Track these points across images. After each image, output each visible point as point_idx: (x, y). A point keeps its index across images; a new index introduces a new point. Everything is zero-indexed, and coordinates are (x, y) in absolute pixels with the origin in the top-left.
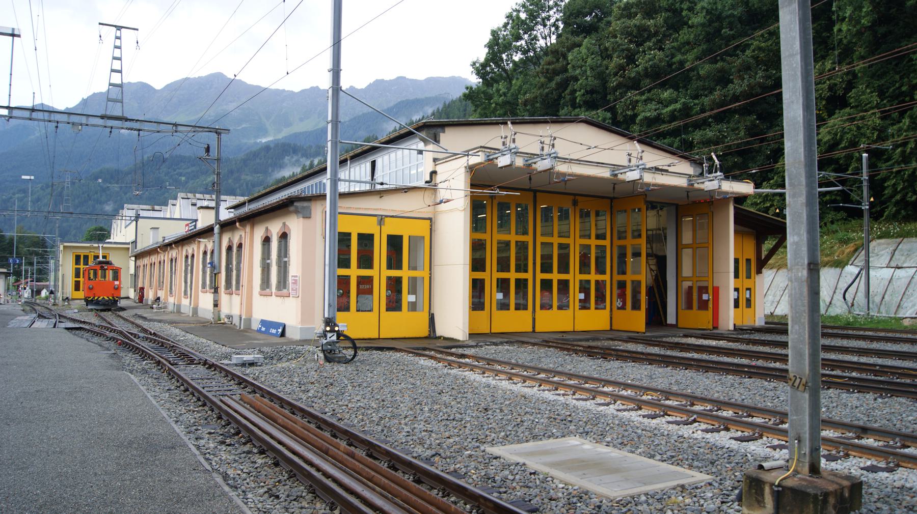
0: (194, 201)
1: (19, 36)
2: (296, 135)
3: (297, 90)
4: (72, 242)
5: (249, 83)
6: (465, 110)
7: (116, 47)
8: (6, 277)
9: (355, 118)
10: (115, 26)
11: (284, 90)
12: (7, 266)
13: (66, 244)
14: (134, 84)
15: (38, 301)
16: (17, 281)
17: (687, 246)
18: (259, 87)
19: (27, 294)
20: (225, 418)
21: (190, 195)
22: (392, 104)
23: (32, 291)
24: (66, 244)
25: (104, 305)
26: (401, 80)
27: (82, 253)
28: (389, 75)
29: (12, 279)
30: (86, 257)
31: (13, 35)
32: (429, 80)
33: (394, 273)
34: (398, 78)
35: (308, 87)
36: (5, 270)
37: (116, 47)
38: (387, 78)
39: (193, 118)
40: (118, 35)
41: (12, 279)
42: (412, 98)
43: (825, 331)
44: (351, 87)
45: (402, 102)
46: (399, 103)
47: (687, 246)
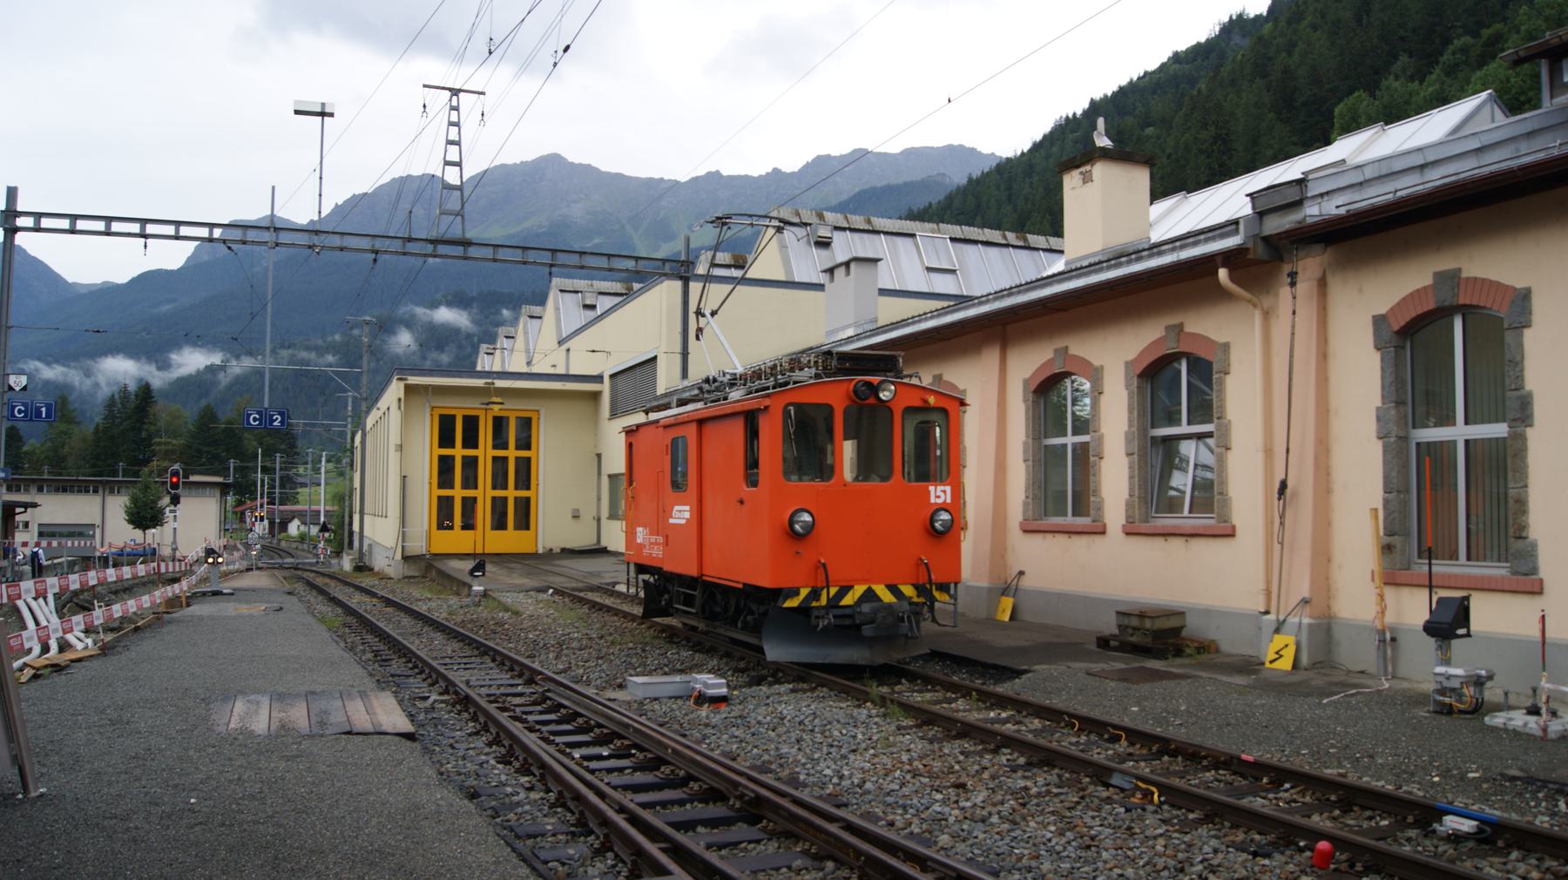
0: (824, 232)
1: (331, 115)
3: (683, 176)
5: (603, 169)
6: (1009, 188)
7: (451, 124)
8: (224, 494)
10: (450, 89)
12: (224, 472)
15: (283, 544)
16: (240, 503)
17: (211, 233)
19: (261, 528)
20: (493, 730)
23: (272, 523)
26: (860, 155)
27: (459, 408)
28: (839, 147)
30: (471, 424)
31: (323, 114)
32: (909, 153)
33: (470, 493)
36: (219, 479)
37: (451, 124)
38: (835, 152)
39: (513, 230)
40: (454, 103)
41: (230, 499)
42: (880, 184)
43: (1115, 480)
44: (775, 170)
45: (865, 191)
47: (211, 233)
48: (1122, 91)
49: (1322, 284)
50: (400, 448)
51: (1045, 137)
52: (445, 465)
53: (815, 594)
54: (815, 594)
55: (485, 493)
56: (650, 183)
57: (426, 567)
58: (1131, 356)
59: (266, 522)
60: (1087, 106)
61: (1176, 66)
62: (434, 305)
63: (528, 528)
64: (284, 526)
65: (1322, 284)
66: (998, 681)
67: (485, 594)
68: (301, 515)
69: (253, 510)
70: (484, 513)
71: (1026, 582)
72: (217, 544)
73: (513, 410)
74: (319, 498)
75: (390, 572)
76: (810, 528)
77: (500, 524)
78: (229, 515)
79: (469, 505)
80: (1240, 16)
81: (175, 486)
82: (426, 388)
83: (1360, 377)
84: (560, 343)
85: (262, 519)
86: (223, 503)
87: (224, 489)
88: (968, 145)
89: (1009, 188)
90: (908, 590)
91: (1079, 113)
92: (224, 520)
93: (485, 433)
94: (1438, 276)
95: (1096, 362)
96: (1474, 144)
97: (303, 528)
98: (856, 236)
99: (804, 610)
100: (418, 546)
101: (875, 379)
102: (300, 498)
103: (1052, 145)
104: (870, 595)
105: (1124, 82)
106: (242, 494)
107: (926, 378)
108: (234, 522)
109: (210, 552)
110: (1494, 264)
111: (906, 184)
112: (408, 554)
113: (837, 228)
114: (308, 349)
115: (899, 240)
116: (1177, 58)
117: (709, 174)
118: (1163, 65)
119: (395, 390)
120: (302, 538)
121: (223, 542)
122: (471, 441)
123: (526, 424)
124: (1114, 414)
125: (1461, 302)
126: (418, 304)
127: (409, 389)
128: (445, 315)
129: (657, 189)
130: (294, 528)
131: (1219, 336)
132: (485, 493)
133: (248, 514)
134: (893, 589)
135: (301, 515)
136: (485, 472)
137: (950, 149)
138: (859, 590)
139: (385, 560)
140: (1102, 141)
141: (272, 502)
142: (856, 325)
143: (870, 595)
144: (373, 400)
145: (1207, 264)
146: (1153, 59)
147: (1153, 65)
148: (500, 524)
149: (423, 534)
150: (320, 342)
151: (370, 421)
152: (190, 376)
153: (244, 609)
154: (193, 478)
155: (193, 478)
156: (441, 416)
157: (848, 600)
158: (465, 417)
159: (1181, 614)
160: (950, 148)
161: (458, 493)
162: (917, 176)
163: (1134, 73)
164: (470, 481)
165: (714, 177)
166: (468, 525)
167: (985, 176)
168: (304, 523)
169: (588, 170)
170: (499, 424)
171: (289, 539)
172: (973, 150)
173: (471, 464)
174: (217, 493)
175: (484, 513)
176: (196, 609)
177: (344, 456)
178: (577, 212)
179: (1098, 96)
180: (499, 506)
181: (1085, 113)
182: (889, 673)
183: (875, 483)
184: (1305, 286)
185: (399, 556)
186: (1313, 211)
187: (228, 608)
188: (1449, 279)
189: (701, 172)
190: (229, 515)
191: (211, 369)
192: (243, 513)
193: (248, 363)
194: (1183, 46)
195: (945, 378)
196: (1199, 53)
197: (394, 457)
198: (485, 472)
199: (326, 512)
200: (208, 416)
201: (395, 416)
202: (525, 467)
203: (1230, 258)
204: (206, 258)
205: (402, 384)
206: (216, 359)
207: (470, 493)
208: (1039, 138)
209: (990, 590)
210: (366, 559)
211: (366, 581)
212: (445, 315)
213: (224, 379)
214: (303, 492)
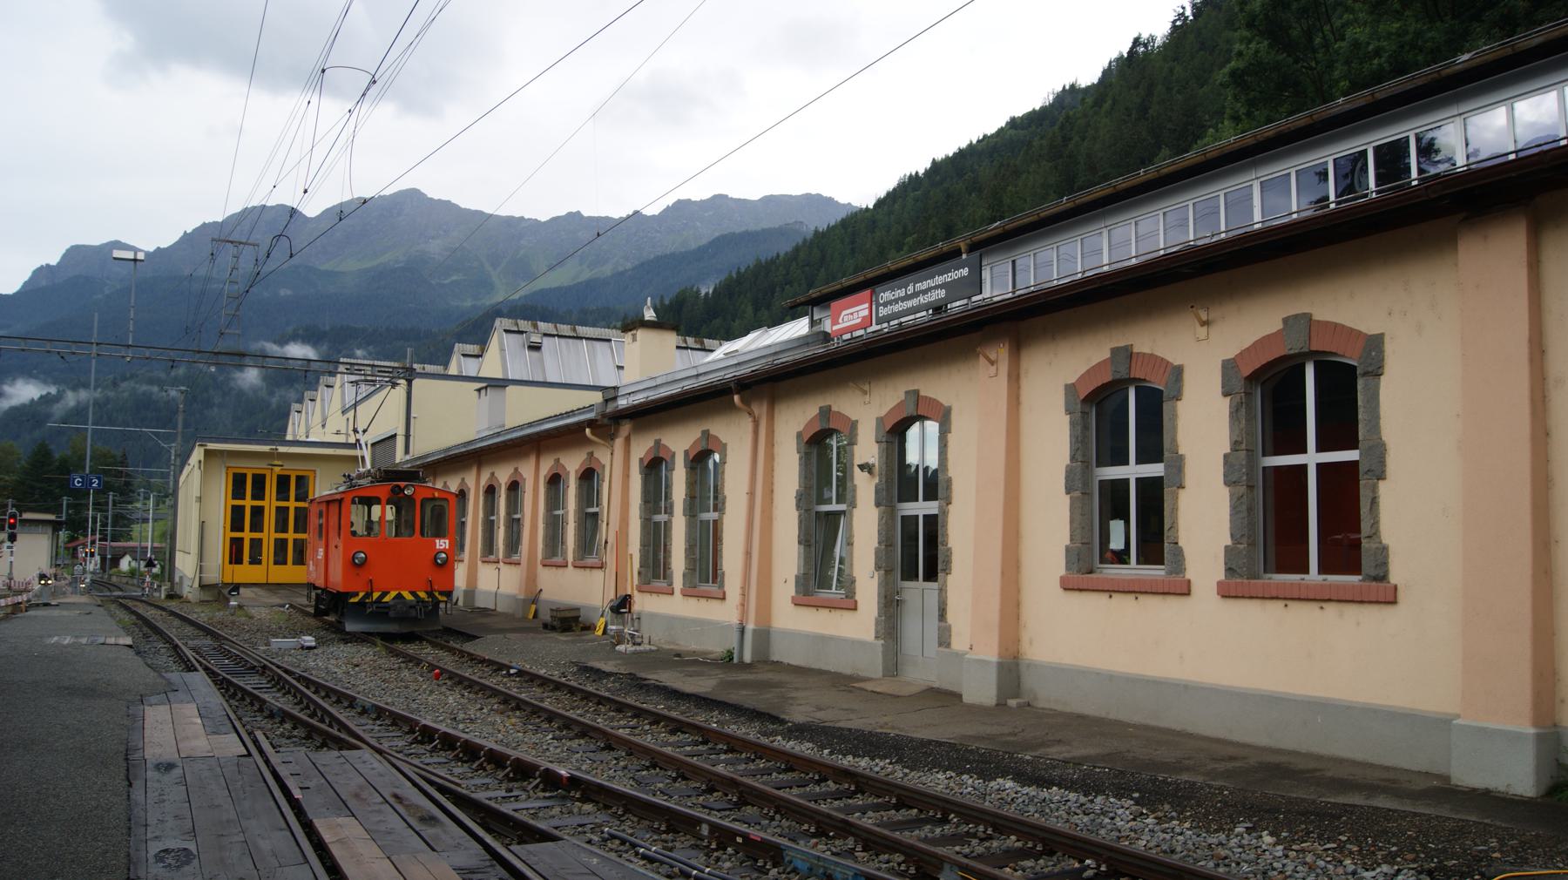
0: (535, 338)
2: (543, 293)
3: (543, 218)
4: (225, 441)
6: (853, 242)
9: (642, 264)
11: (522, 218)
12: (56, 510)
13: (212, 446)
14: (272, 208)
15: (114, 579)
16: (72, 539)
18: (482, 213)
19: (93, 564)
21: (524, 325)
22: (704, 242)
23: (103, 559)
24: (212, 446)
25: (401, 619)
26: (719, 202)
27: (250, 468)
29: (63, 535)
30: (259, 482)
32: (769, 201)
33: (257, 535)
34: (715, 197)
35: (563, 213)
36: (52, 517)
41: (63, 535)
42: (738, 230)
45: (723, 237)
46: (717, 239)
48: (961, 154)
49: (628, 440)
50: (200, 499)
51: (888, 194)
52: (237, 512)
53: (368, 595)
54: (368, 595)
55: (269, 535)
56: (510, 222)
57: (218, 593)
58: (1072, 379)
59: (98, 558)
60: (928, 166)
61: (1012, 132)
62: (283, 342)
63: (260, 562)
64: (115, 561)
65: (628, 440)
66: (463, 642)
67: (240, 607)
68: (132, 552)
69: (85, 546)
70: (268, 551)
71: (543, 596)
72: (49, 571)
73: (293, 469)
74: (146, 536)
75: (190, 597)
76: (364, 562)
77: (280, 559)
78: (61, 551)
79: (256, 545)
80: (1072, 86)
81: (12, 526)
82: (222, 452)
83: (1051, 438)
84: (343, 413)
85: (92, 555)
86: (55, 537)
87: (56, 526)
88: (826, 194)
89: (853, 242)
90: (422, 595)
91: (921, 172)
92: (55, 555)
93: (271, 488)
94: (1114, 351)
95: (945, 402)
96: (694, 372)
97: (134, 564)
98: (563, 341)
99: (361, 603)
100: (213, 576)
101: (402, 484)
102: (135, 534)
103: (894, 202)
104: (399, 596)
105: (964, 145)
106: (76, 531)
107: (439, 485)
108: (65, 556)
109: (42, 577)
110: (1349, 306)
111: (763, 230)
112: (205, 582)
113: (546, 335)
114: (151, 382)
115: (598, 345)
116: (1013, 123)
117: (570, 214)
118: (1001, 130)
119: (197, 454)
120: (132, 573)
121: (53, 571)
122: (259, 493)
123: (301, 480)
124: (1205, 427)
125: (1314, 348)
126: (267, 340)
127: (208, 453)
128: (297, 350)
129: (515, 227)
130: (125, 564)
131: (1369, 327)
132: (269, 535)
133: (80, 549)
134: (413, 593)
135: (132, 552)
136: (270, 519)
137: (808, 198)
138: (393, 594)
139: (189, 590)
140: (649, 315)
141: (103, 539)
142: (489, 429)
143: (399, 596)
144: (184, 462)
145: (578, 428)
146: (990, 122)
147: (991, 130)
148: (280, 559)
149: (217, 568)
150: (163, 375)
151: (182, 479)
152: (24, 406)
153: (65, 613)
154: (26, 516)
155: (26, 516)
156: (235, 475)
157: (386, 599)
158: (254, 476)
159: (578, 609)
160: (808, 197)
161: (247, 535)
162: (775, 223)
163: (974, 136)
164: (257, 526)
165: (575, 217)
166: (255, 561)
167: (830, 229)
168: (135, 559)
169: (448, 205)
170: (283, 482)
171: (120, 574)
172: (831, 199)
173: (258, 512)
174: (50, 531)
175: (268, 551)
176: (31, 613)
177: (168, 496)
178: (435, 248)
179: (940, 156)
180: (281, 545)
181: (927, 172)
182: (409, 638)
183: (405, 539)
184: (619, 442)
185: (196, 585)
186: (623, 403)
187: (56, 612)
188: (1125, 355)
189: (562, 212)
190: (61, 551)
191: (45, 400)
192: (75, 549)
193: (83, 395)
194: (1019, 112)
195: (835, 408)
196: (1035, 119)
197: (195, 506)
198: (270, 519)
199: (153, 548)
200: (42, 457)
201: (197, 474)
202: (237, 524)
203: (591, 423)
204: (44, 283)
205: (202, 450)
206: (53, 390)
207: (257, 535)
208: (882, 194)
209: (524, 601)
210: (177, 589)
211: (173, 605)
212: (297, 350)
213: (58, 410)
214: (136, 528)
